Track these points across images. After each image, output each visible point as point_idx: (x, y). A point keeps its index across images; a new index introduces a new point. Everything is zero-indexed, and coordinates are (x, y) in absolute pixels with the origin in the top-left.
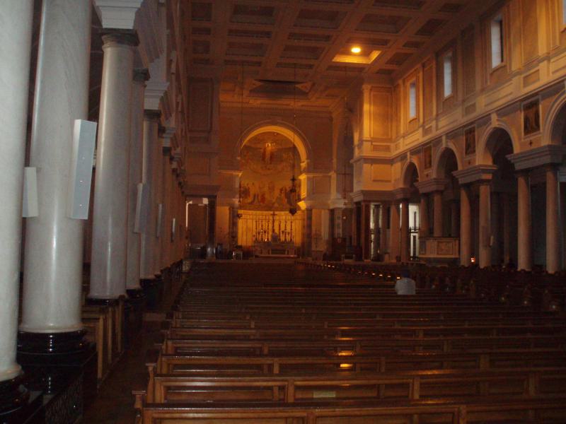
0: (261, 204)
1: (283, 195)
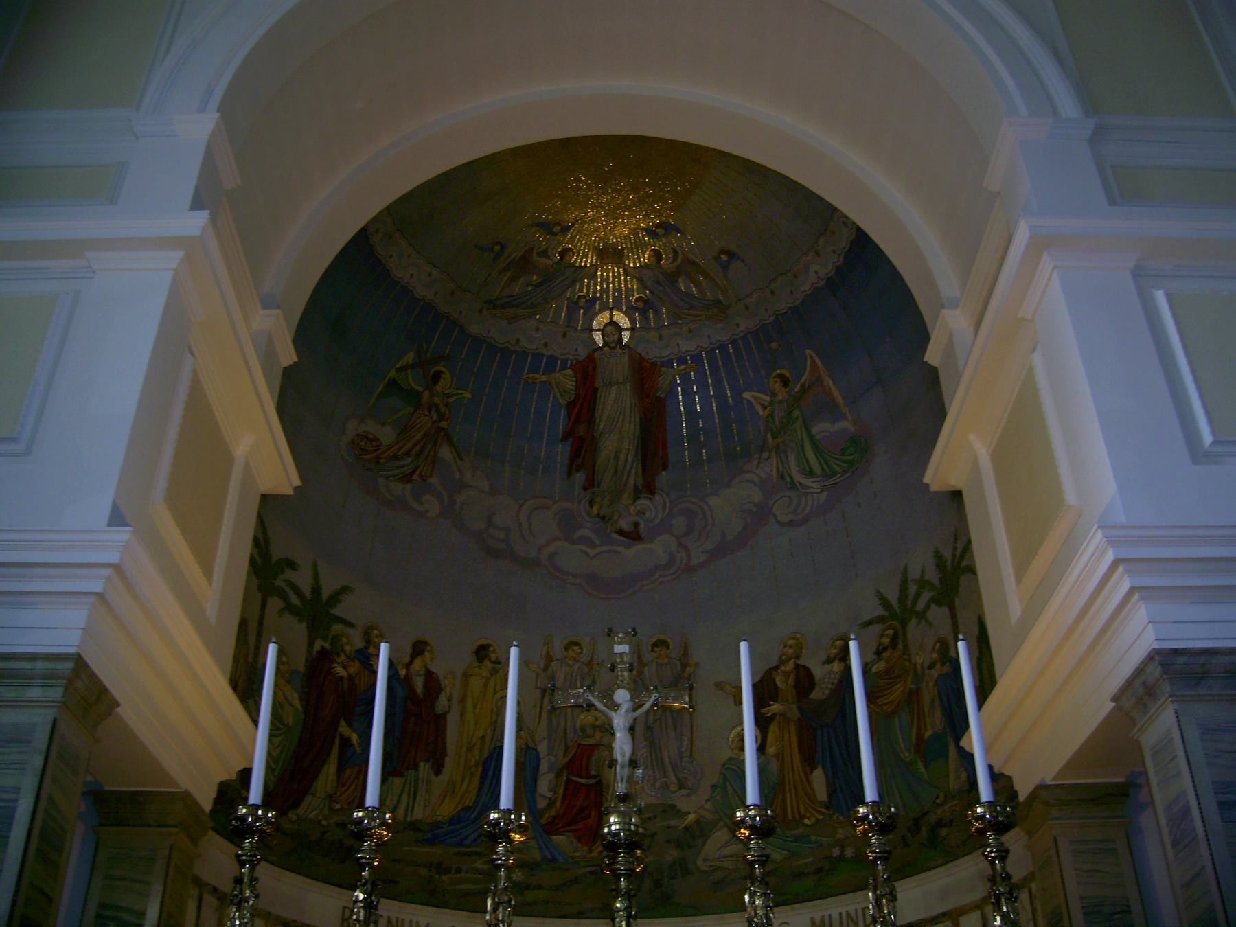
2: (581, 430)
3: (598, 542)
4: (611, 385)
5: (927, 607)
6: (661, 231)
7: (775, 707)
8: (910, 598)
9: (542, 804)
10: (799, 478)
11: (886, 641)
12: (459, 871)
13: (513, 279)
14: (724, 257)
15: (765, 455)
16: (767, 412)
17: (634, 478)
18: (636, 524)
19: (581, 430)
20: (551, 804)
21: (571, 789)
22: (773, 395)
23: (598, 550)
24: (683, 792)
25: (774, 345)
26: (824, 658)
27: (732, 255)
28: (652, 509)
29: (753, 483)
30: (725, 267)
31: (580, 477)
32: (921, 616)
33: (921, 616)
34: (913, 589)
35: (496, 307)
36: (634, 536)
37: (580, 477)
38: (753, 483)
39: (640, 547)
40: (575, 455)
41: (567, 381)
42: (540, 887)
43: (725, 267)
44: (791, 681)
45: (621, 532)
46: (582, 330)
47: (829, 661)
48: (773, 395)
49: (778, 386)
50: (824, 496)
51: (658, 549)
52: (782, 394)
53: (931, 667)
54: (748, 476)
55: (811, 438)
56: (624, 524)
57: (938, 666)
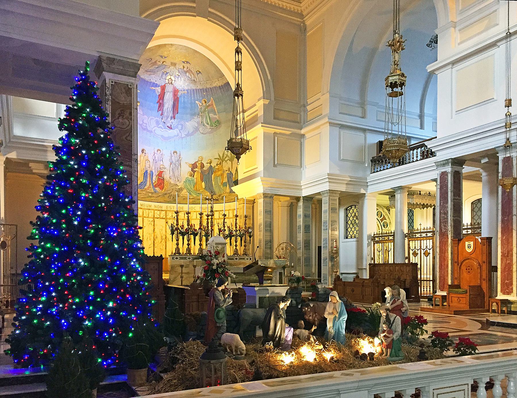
0: (157, 189)
1: (197, 175)
2: (161, 101)
3: (163, 128)
4: (168, 92)
5: (227, 160)
6: (186, 63)
7: (196, 169)
8: (224, 157)
9: (154, 182)
10: (205, 124)
11: (219, 163)
12: (141, 194)
13: (152, 66)
14: (198, 72)
15: (199, 116)
16: (200, 107)
17: (171, 114)
18: (171, 125)
19: (161, 101)
20: (155, 182)
21: (159, 179)
22: (202, 104)
23: (163, 130)
24: (179, 182)
25: (205, 94)
26: (207, 162)
27: (200, 72)
28: (174, 122)
29: (195, 121)
30: (198, 74)
31: (160, 112)
32: (226, 161)
33: (226, 161)
34: (225, 156)
35: (147, 72)
36: (170, 128)
37: (160, 112)
38: (195, 121)
39: (171, 130)
40: (159, 107)
41: (159, 89)
42: (154, 197)
43: (198, 74)
44: (200, 165)
45: (168, 127)
46: (164, 79)
47: (207, 163)
48: (202, 104)
49: (204, 102)
50: (210, 130)
51: (175, 132)
52: (204, 104)
53: (226, 171)
54: (195, 120)
55: (209, 116)
56: (169, 125)
57: (228, 171)
